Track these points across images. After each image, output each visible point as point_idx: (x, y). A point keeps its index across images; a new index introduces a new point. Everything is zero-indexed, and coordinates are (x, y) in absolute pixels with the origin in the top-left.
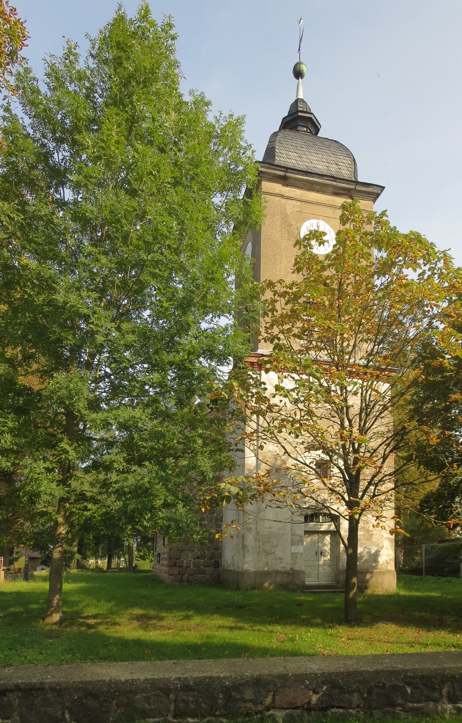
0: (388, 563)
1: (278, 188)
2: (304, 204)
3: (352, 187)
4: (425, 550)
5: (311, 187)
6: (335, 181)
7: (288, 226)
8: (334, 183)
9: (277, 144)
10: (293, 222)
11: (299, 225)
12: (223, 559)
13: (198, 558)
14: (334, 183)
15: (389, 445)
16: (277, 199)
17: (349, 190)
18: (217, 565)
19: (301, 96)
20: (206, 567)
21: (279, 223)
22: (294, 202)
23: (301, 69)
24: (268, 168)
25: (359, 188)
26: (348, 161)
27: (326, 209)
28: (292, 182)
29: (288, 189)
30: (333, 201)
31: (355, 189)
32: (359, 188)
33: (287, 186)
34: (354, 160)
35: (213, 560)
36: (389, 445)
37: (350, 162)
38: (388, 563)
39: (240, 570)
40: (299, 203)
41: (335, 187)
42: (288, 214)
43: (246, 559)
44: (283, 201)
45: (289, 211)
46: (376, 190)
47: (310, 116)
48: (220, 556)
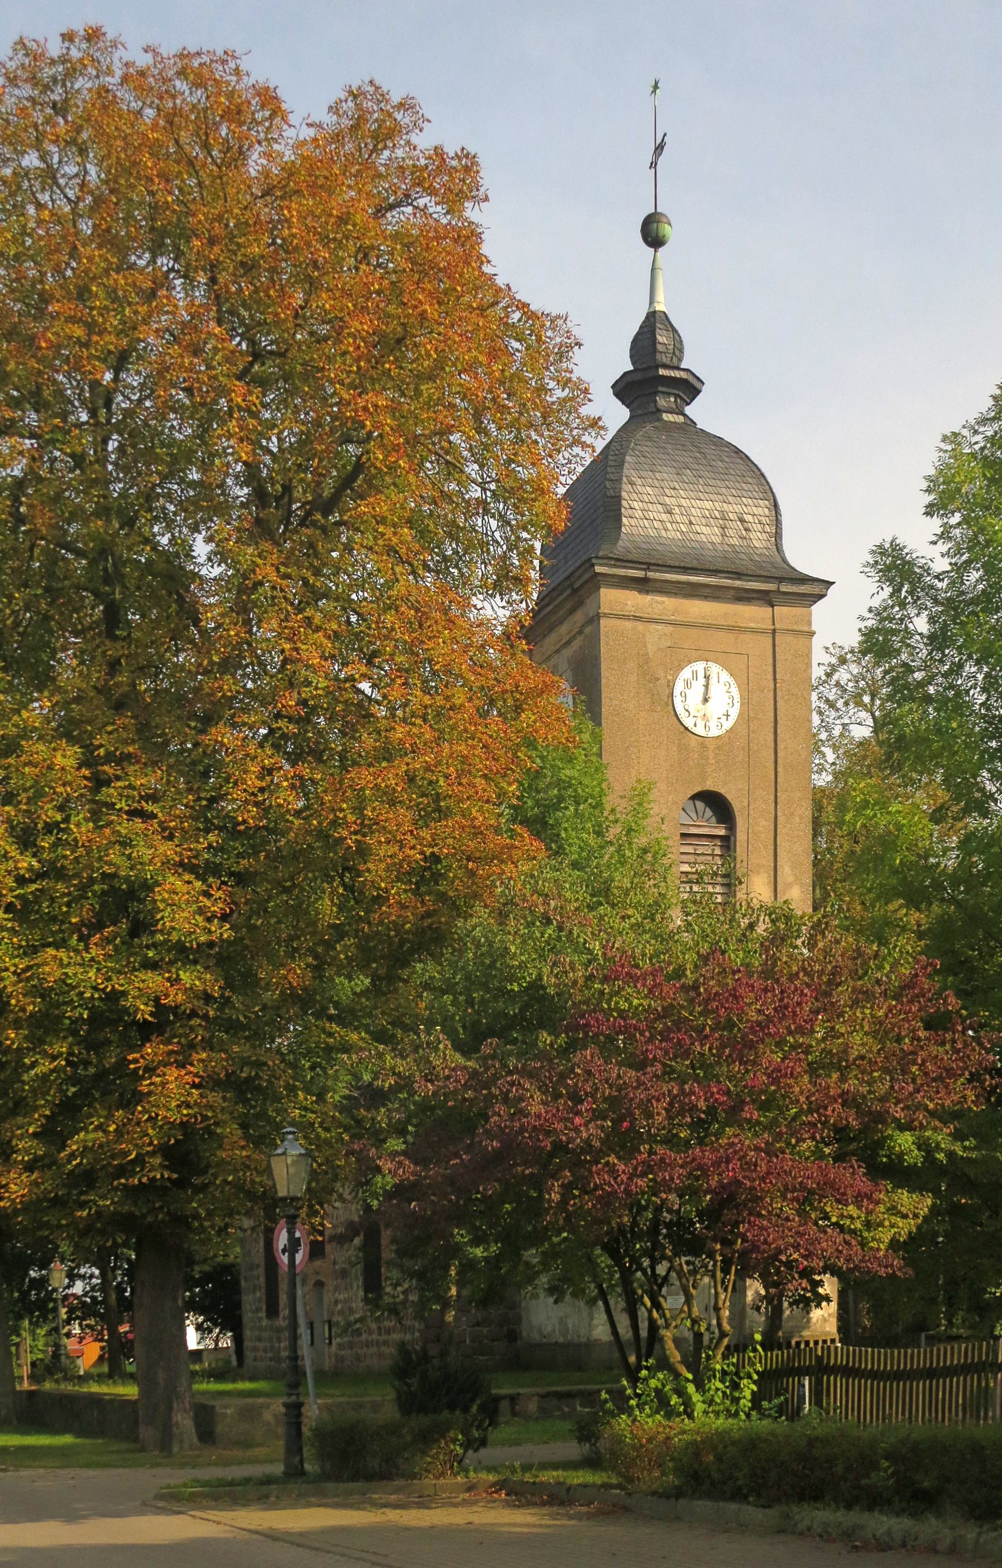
0: (825, 1320)
1: (631, 600)
2: (679, 629)
3: (771, 587)
4: (519, 1394)
5: (693, 591)
6: (739, 579)
7: (650, 682)
8: (738, 583)
9: (624, 486)
10: (661, 674)
11: (670, 677)
12: (524, 1325)
13: (478, 1324)
14: (738, 583)
15: (835, 1411)
16: (629, 624)
17: (766, 592)
18: (513, 1336)
19: (660, 307)
20: (494, 1340)
21: (633, 678)
22: (659, 627)
23: (661, 234)
24: (615, 566)
25: (784, 588)
26: (763, 509)
27: (721, 634)
28: (657, 585)
29: (649, 598)
30: (735, 614)
31: (778, 591)
32: (784, 588)
33: (647, 592)
34: (776, 505)
35: (505, 1328)
36: (835, 1411)
37: (766, 511)
38: (825, 1320)
39: (584, 1340)
40: (670, 628)
41: (737, 589)
42: (650, 655)
43: (595, 1322)
44: (640, 626)
45: (651, 649)
46: (816, 589)
47: (683, 375)
48: (519, 1320)
